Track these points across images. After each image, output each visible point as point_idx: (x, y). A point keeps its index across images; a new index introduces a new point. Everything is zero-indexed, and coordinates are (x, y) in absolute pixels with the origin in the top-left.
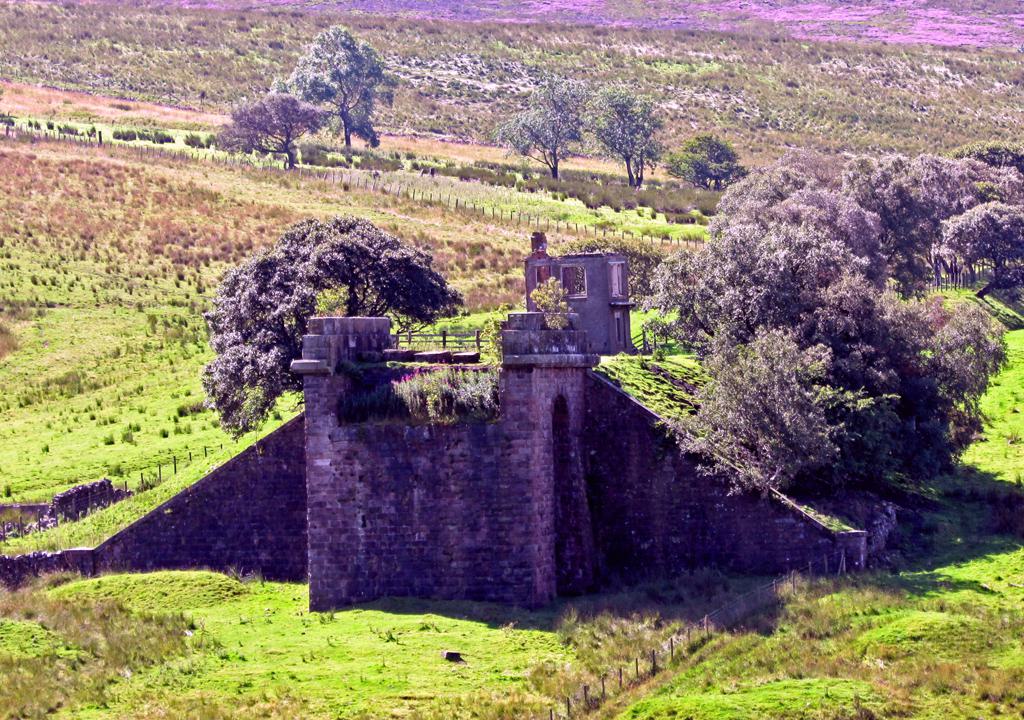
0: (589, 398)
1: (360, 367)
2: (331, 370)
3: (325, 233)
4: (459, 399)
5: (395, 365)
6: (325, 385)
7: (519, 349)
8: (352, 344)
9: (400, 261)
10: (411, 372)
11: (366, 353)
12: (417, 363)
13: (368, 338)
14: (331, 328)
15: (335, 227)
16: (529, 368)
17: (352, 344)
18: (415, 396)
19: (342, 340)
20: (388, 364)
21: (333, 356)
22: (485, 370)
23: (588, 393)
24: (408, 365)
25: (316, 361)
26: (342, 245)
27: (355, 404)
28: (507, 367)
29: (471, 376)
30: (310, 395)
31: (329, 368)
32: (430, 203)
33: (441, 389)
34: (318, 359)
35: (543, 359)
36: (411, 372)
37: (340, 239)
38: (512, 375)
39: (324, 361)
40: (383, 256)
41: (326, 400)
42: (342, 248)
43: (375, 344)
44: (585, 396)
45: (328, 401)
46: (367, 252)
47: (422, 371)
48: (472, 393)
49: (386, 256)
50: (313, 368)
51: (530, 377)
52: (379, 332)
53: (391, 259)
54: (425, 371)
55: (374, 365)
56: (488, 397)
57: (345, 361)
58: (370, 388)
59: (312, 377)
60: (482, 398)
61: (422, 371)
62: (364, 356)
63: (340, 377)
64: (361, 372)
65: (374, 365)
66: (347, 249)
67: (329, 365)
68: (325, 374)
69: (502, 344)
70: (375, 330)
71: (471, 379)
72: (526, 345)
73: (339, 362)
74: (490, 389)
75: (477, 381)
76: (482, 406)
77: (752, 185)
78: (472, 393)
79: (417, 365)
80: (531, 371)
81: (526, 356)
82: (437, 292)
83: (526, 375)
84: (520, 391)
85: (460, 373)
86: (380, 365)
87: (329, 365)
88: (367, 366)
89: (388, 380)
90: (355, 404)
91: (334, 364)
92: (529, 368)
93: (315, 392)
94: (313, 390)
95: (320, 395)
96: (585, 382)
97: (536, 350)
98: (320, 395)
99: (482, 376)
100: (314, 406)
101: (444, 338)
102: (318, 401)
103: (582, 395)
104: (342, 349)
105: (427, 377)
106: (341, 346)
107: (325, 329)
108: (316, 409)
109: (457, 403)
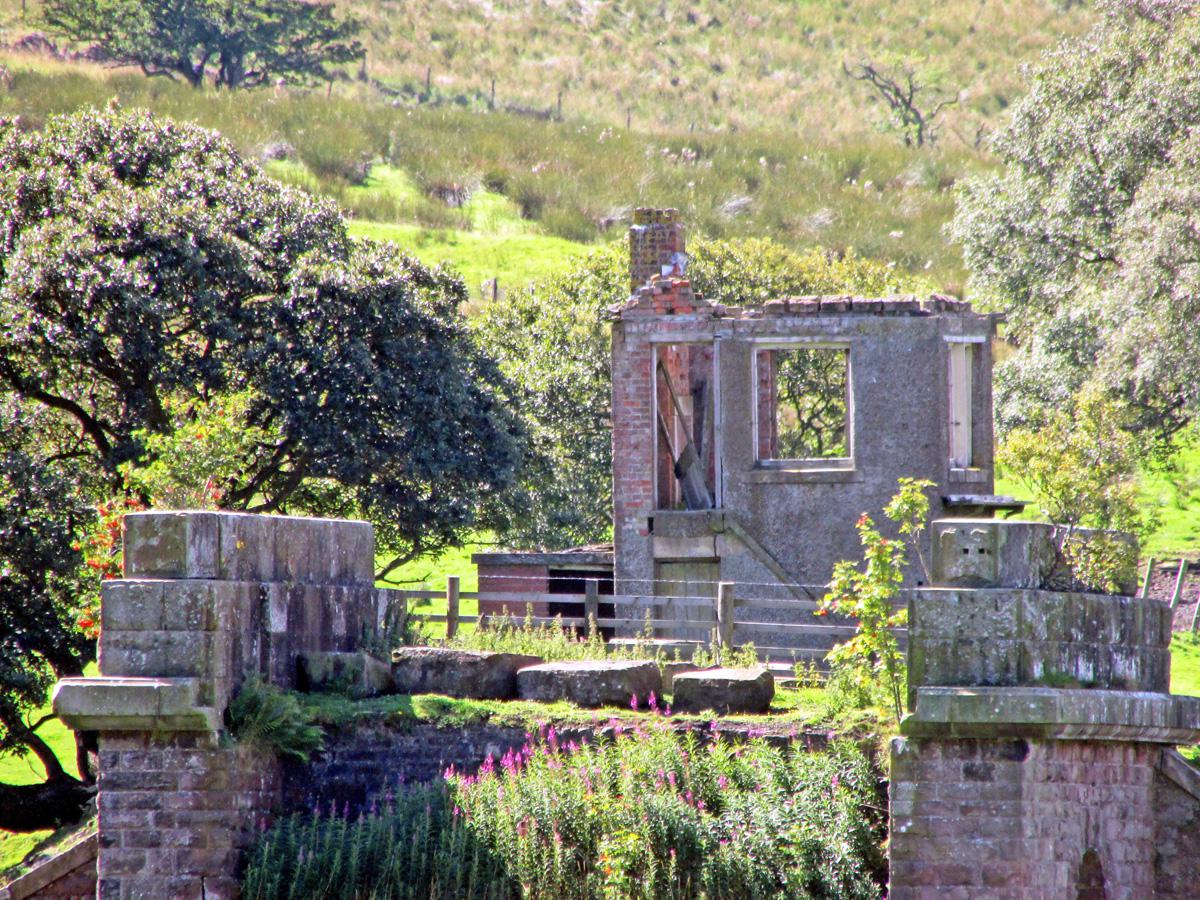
0: (1171, 869)
1: (313, 712)
2: (212, 717)
3: (58, 176)
4: (727, 853)
5: (445, 708)
6: (185, 781)
7: (975, 663)
8: (277, 623)
9: (361, 302)
10: (515, 741)
11: (319, 664)
12: (529, 705)
13: (323, 595)
14: (209, 552)
15: (91, 156)
16: (1016, 740)
17: (277, 623)
18: (543, 834)
19: (246, 603)
20: (419, 705)
21: (220, 667)
22: (816, 741)
23: (1170, 848)
24: (502, 711)
25: (156, 684)
26: (138, 229)
27: (305, 858)
28: (925, 735)
29: (760, 761)
30: (124, 818)
31: (205, 710)
32: (1087, 97)
33: (652, 813)
34: (162, 675)
35: (1071, 708)
36: (515, 741)
37: (126, 204)
38: (942, 764)
39: (191, 683)
40: (293, 276)
41: (185, 839)
42: (140, 242)
43: (340, 628)
44: (1157, 861)
45: (197, 842)
46: (233, 258)
47: (567, 739)
48: (772, 830)
49: (310, 280)
50: (144, 710)
51: (1016, 777)
52: (345, 576)
53: (330, 291)
54: (574, 736)
55: (364, 708)
56: (841, 848)
57: (256, 686)
58: (353, 800)
59: (132, 746)
60: (815, 853)
61: (567, 739)
62: (316, 672)
63: (242, 750)
64: (316, 732)
65: (364, 708)
66: (157, 244)
67: (203, 701)
68: (188, 737)
69: (907, 643)
70: (333, 572)
71: (766, 776)
72: (1003, 649)
73: (236, 692)
74: (843, 818)
75: (789, 789)
76: (816, 887)
77: (1138, 62)
78: (772, 830)
79: (532, 712)
80: (1020, 751)
81: (1009, 693)
82: (500, 427)
83: (1001, 766)
84: (974, 831)
85: (718, 752)
86: (388, 705)
87: (203, 701)
88: (335, 707)
89: (424, 768)
90: (305, 858)
91: (220, 695)
92: (1016, 740)
93: (143, 805)
94: (135, 796)
95: (163, 820)
96: (1158, 806)
97: (1038, 671)
98: (163, 820)
99: (809, 765)
100: (139, 864)
101: (453, 607)
102: (155, 844)
103: (1148, 854)
104: (244, 642)
105: (583, 759)
106: (244, 626)
107: (191, 556)
108: (144, 873)
109: (719, 873)
